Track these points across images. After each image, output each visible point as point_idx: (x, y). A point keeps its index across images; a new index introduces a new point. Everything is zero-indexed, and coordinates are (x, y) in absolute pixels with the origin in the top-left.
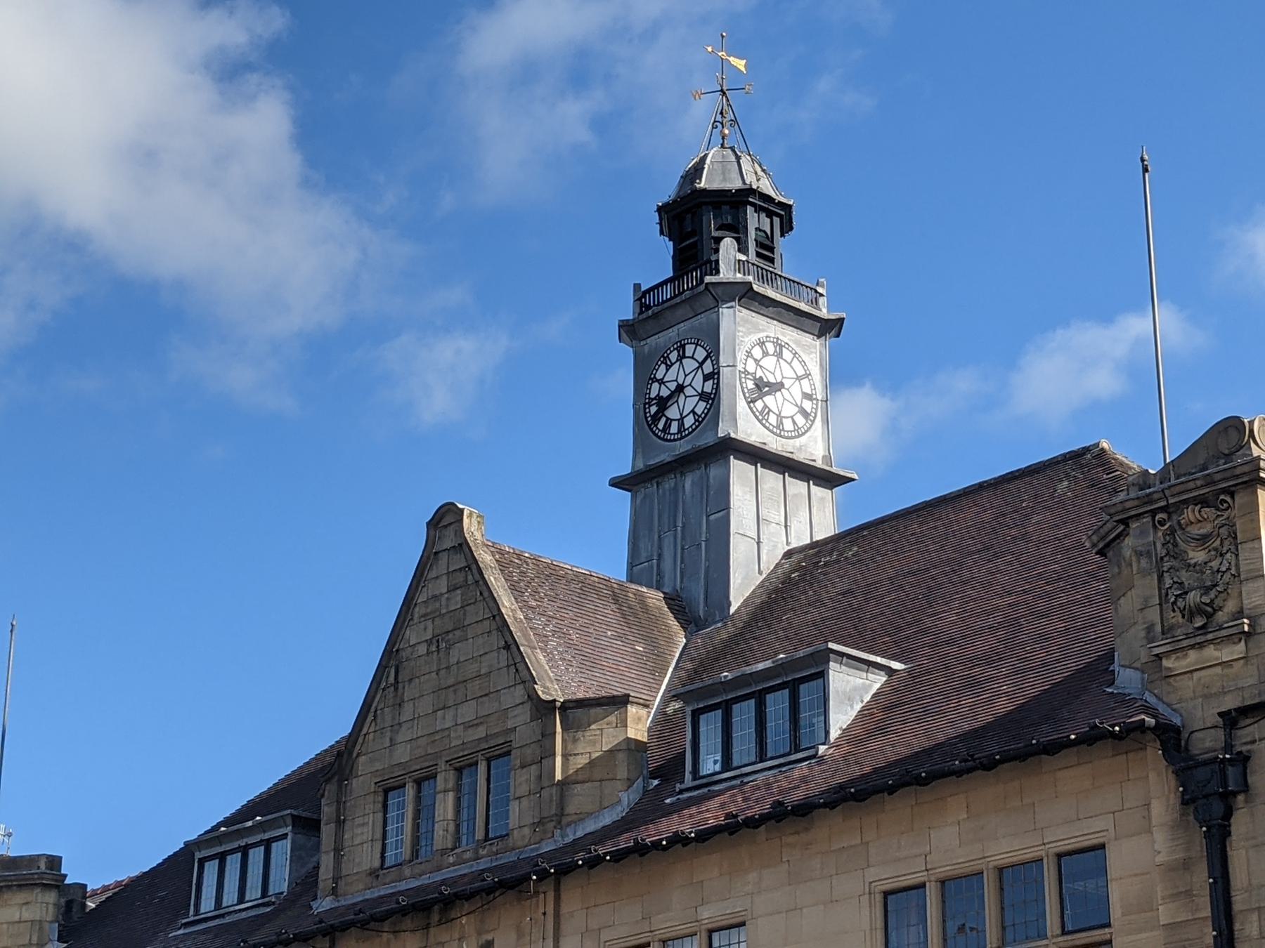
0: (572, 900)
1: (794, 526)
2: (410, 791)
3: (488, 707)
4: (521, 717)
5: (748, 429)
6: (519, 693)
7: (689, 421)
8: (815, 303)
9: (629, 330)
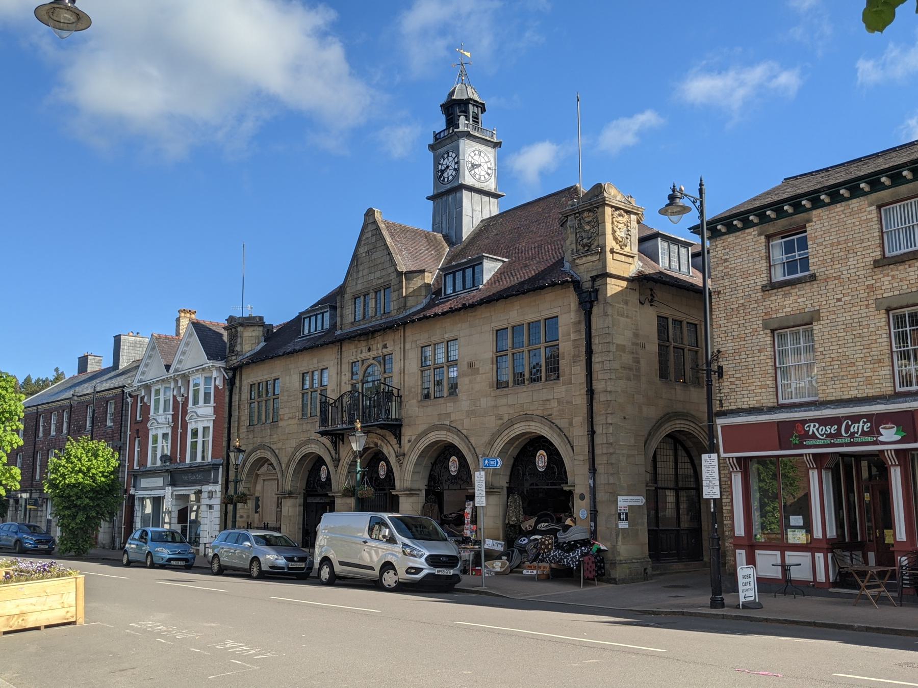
0: (409, 332)
2: (362, 298)
3: (384, 273)
4: (394, 276)
5: (468, 180)
6: (393, 269)
7: (450, 178)
8: (492, 136)
9: (432, 147)
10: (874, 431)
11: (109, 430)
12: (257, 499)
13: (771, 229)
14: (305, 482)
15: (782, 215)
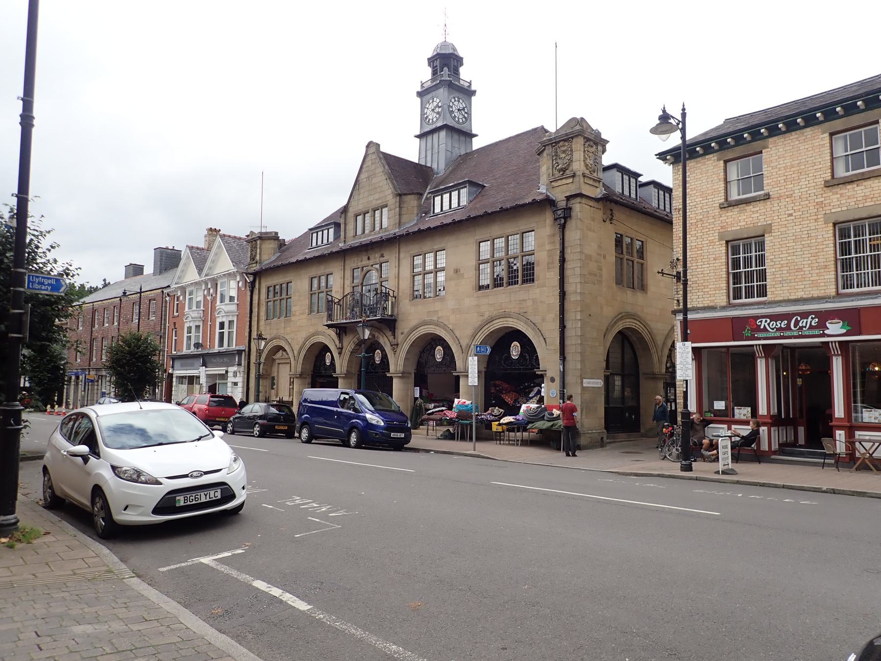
9: (420, 94)
10: (822, 325)
11: (152, 323)
12: (273, 378)
13: (730, 155)
14: (313, 365)
15: (743, 139)
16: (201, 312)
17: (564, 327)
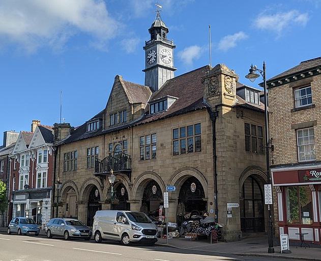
1: (168, 77)
4: (128, 105)
16: (29, 168)
17: (216, 175)
